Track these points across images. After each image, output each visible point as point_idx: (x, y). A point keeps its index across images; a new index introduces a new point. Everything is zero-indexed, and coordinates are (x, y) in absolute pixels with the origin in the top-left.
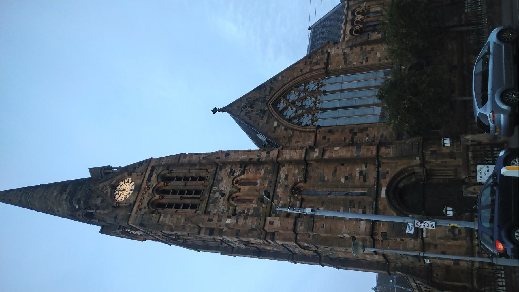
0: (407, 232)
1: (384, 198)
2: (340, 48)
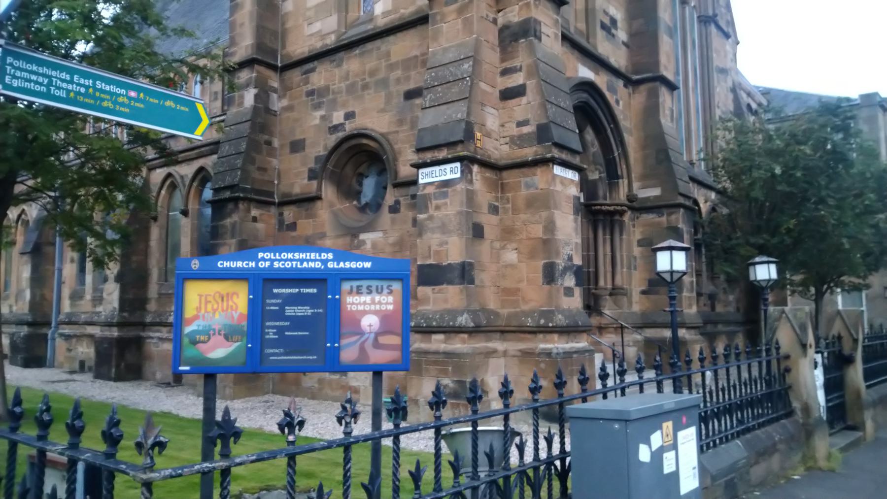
1: (577, 71)
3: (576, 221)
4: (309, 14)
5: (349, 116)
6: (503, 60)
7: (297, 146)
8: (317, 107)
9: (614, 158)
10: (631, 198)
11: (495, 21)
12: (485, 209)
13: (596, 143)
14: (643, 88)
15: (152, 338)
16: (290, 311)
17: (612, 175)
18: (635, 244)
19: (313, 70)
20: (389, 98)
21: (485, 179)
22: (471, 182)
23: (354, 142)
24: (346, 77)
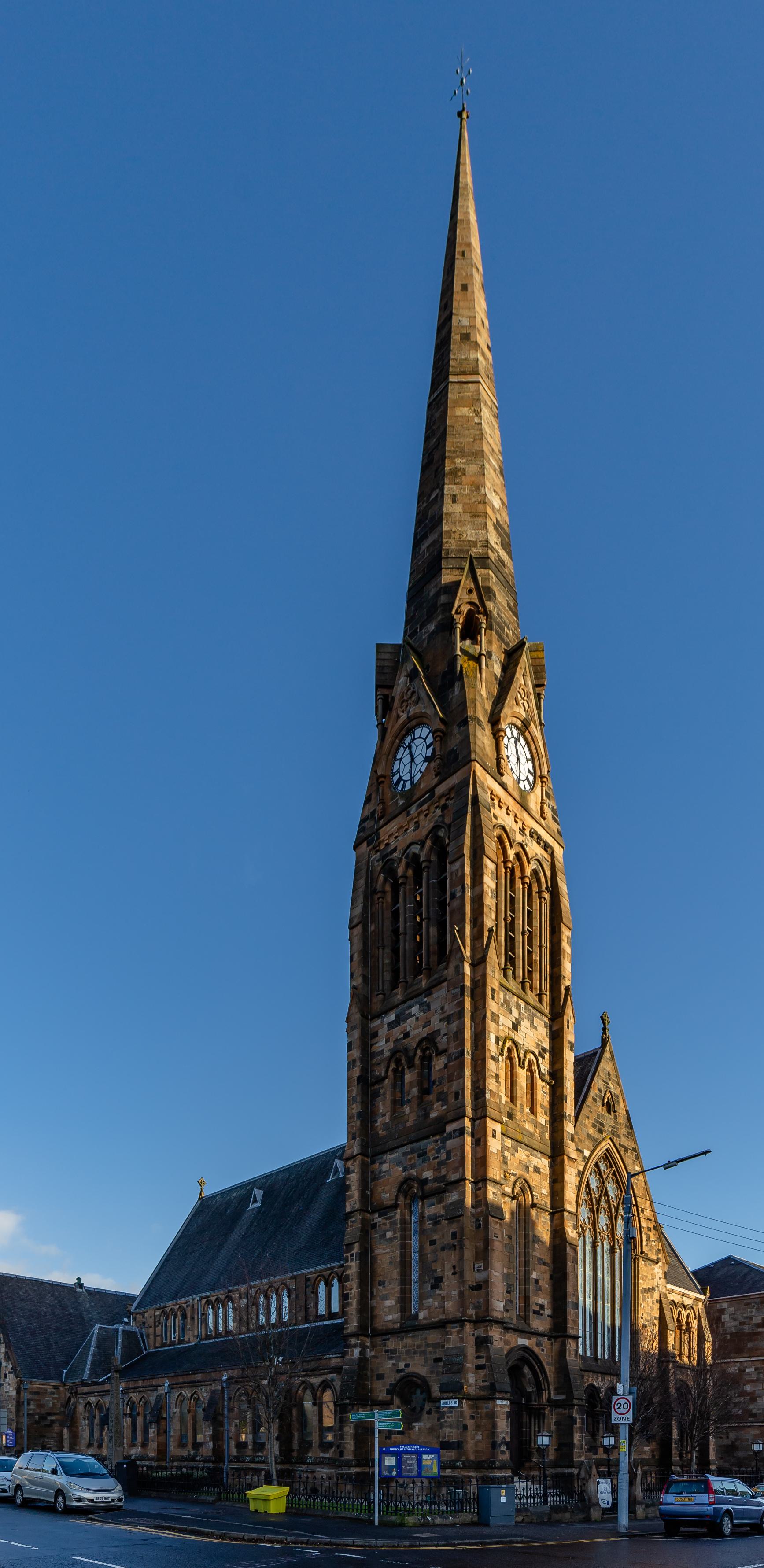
0: (394, 1464)
1: (517, 1342)
2: (660, 1282)
3: (507, 1422)
4: (386, 1310)
5: (407, 1366)
6: (477, 1352)
7: (380, 1377)
8: (391, 1358)
9: (540, 1381)
10: (549, 1400)
11: (474, 1335)
12: (468, 1417)
13: (530, 1373)
14: (559, 1340)
15: (297, 1471)
16: (408, 1462)
17: (539, 1390)
18: (552, 1424)
19: (388, 1339)
20: (426, 1359)
21: (468, 1405)
22: (462, 1407)
23: (409, 1378)
24: (406, 1347)
